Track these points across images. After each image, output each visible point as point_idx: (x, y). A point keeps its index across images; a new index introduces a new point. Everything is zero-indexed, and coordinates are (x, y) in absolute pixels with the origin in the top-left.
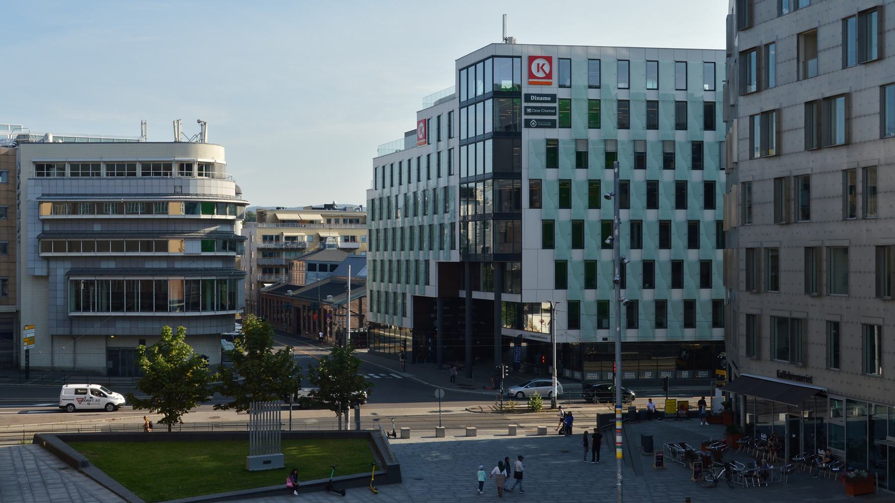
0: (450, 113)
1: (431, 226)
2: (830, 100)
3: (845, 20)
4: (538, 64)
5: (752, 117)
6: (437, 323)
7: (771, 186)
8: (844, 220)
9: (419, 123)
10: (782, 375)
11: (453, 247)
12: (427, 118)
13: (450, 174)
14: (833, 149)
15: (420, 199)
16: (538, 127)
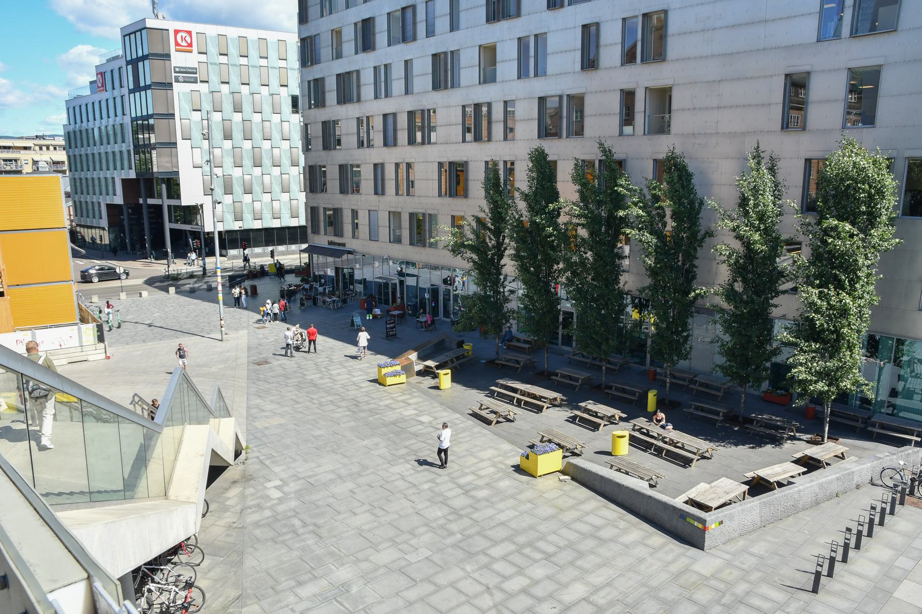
0: (119, 68)
1: (121, 152)
2: (349, 73)
3: (356, 24)
4: (182, 36)
5: (309, 82)
6: (126, 223)
7: (320, 126)
8: (358, 148)
9: (97, 74)
10: (330, 243)
11: (130, 168)
12: (103, 71)
13: (124, 114)
14: (887, 35)
15: (111, 132)
16: (185, 82)
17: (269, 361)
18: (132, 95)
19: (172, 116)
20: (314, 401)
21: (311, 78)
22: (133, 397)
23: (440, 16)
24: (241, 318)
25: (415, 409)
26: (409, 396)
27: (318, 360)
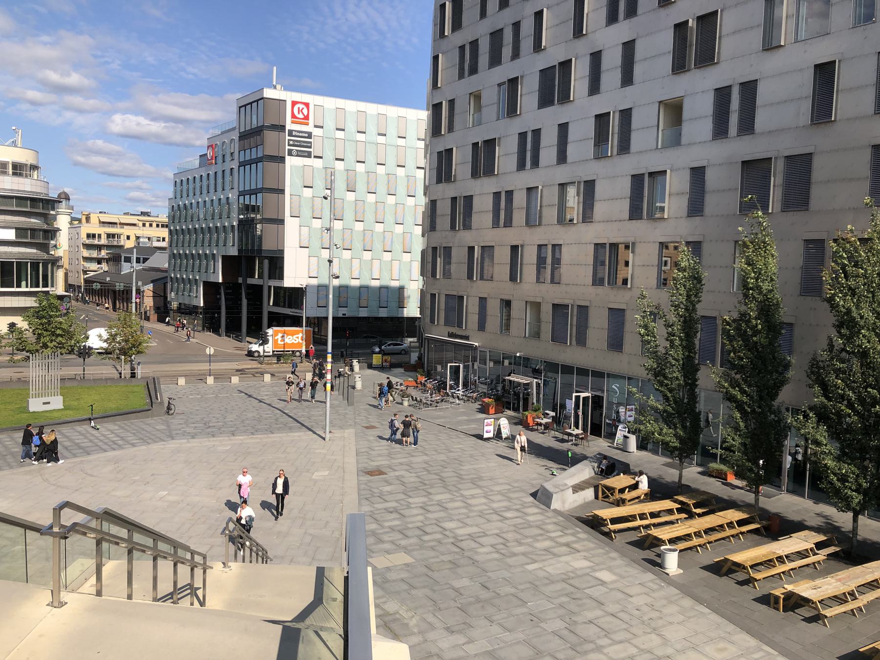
4: (299, 108)
10: (451, 335)
16: (297, 156)
17: (384, 470)
18: (242, 168)
19: (282, 191)
20: (447, 533)
21: (442, 149)
22: (227, 524)
23: (608, 70)
24: (346, 414)
25: (586, 558)
26: (573, 539)
27: (444, 475)
